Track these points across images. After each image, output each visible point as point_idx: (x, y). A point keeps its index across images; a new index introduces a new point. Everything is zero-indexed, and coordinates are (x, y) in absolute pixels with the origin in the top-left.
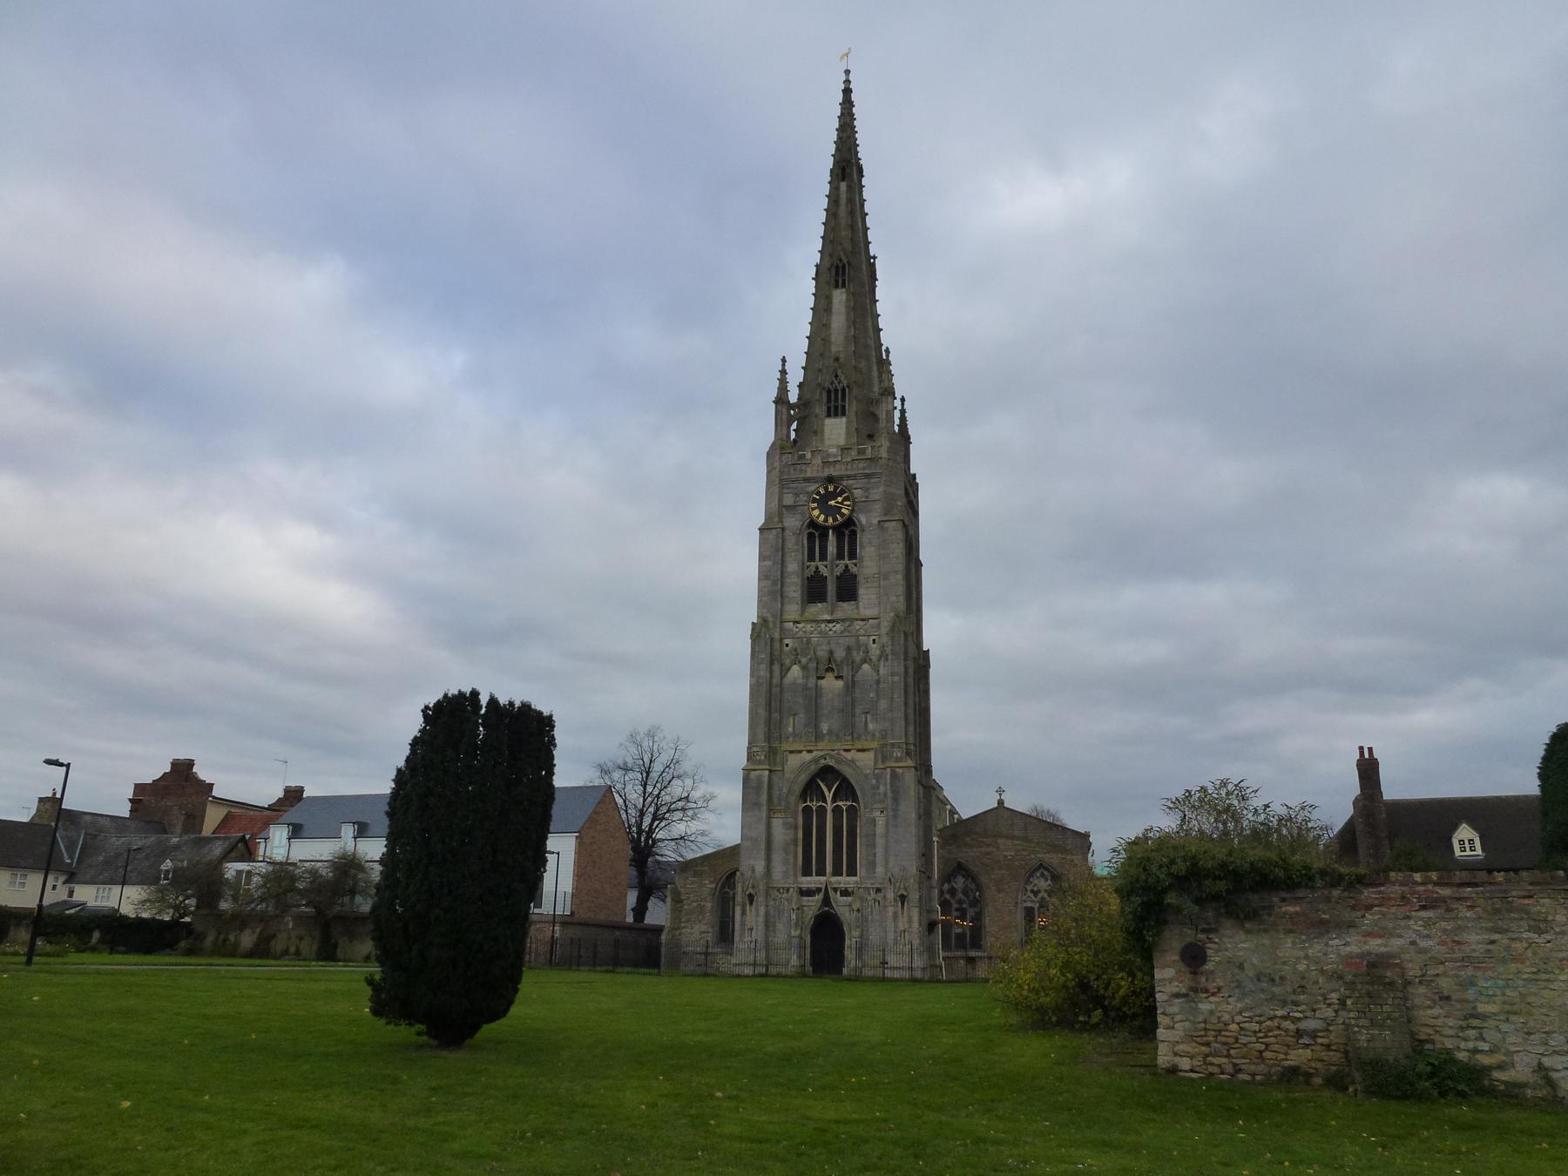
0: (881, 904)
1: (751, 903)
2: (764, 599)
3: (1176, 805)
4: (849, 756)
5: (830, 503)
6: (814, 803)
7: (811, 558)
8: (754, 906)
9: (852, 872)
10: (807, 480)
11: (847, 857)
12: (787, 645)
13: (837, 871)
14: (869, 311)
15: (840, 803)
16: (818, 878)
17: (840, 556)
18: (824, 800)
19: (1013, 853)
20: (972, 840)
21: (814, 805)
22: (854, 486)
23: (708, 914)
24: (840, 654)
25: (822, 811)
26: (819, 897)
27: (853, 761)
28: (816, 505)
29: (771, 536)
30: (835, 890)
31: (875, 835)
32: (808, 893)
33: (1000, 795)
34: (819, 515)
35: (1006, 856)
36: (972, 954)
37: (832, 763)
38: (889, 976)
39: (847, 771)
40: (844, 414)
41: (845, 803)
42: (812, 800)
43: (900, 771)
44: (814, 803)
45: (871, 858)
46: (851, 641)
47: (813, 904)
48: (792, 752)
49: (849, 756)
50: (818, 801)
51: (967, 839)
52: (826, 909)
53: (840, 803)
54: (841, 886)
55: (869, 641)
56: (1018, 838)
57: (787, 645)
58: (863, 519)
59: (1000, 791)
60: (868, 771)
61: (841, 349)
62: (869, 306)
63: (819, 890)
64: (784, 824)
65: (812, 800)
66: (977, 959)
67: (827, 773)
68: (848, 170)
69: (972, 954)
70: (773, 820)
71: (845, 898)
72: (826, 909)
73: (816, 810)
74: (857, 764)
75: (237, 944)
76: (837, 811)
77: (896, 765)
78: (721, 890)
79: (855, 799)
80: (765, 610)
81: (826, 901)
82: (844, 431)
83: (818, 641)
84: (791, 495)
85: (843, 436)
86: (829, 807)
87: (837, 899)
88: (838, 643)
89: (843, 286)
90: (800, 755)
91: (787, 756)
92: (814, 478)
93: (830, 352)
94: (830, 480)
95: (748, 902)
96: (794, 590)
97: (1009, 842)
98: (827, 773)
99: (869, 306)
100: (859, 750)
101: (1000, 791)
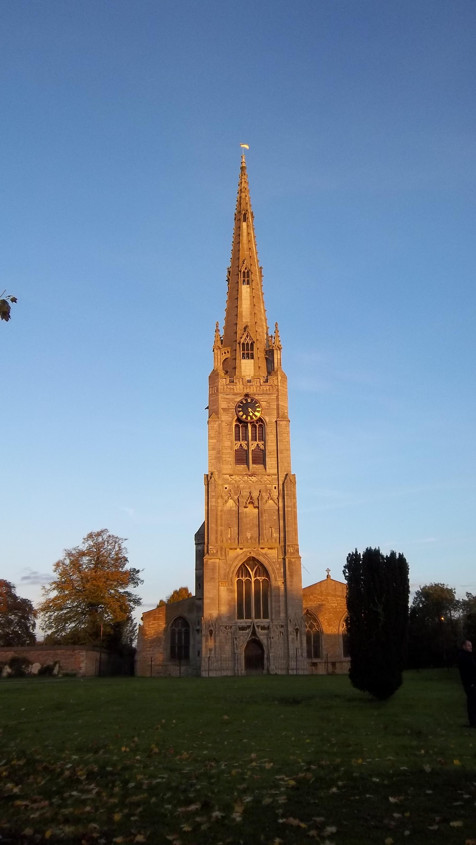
0: (284, 634)
1: (211, 634)
2: (212, 461)
3: (86, 539)
4: (264, 551)
5: (249, 409)
6: (244, 578)
7: (237, 438)
8: (213, 638)
9: (266, 616)
10: (235, 394)
11: (260, 608)
12: (226, 488)
13: (258, 616)
14: (261, 299)
15: (259, 578)
16: (247, 620)
17: (254, 439)
18: (250, 577)
19: (336, 605)
20: (314, 597)
21: (244, 579)
22: (262, 400)
23: (163, 642)
24: (255, 494)
25: (249, 582)
26: (249, 631)
27: (266, 554)
28: (241, 409)
29: (215, 426)
30: (258, 626)
31: (279, 596)
32: (243, 629)
33: (328, 573)
34: (243, 415)
35: (332, 606)
36: (315, 661)
37: (253, 555)
38: (291, 674)
39: (261, 559)
40: (252, 358)
41: (261, 578)
42: (242, 576)
43: (293, 560)
44: (244, 578)
45: (278, 609)
46: (262, 487)
47: (245, 637)
48: (231, 549)
49: (264, 551)
50: (246, 576)
51: (311, 597)
52: (254, 637)
53: (259, 578)
54: (261, 624)
55: (272, 487)
56: (339, 596)
57: (226, 488)
58: (267, 419)
59: (328, 570)
60: (275, 560)
61: (249, 321)
62: (261, 296)
63: (249, 627)
64: (228, 589)
65: (242, 576)
66: (318, 663)
67: (253, 561)
68: (247, 216)
69: (315, 661)
70: (220, 587)
71: (264, 631)
72: (254, 637)
73: (244, 582)
74: (268, 556)
75: (11, 667)
76: (257, 582)
77: (291, 557)
78: (171, 628)
79: (268, 575)
80: (213, 468)
81: (254, 633)
82: (253, 368)
83: (243, 486)
84: (226, 403)
85: (252, 370)
86: (253, 579)
87: (259, 631)
88: (255, 488)
89: (248, 284)
90: (235, 551)
91: (228, 551)
92: (239, 394)
93: (242, 321)
94: (247, 395)
95: (209, 635)
96: (230, 457)
97: (334, 599)
98: (253, 561)
99: (261, 296)
100: (269, 549)
101: (328, 570)
